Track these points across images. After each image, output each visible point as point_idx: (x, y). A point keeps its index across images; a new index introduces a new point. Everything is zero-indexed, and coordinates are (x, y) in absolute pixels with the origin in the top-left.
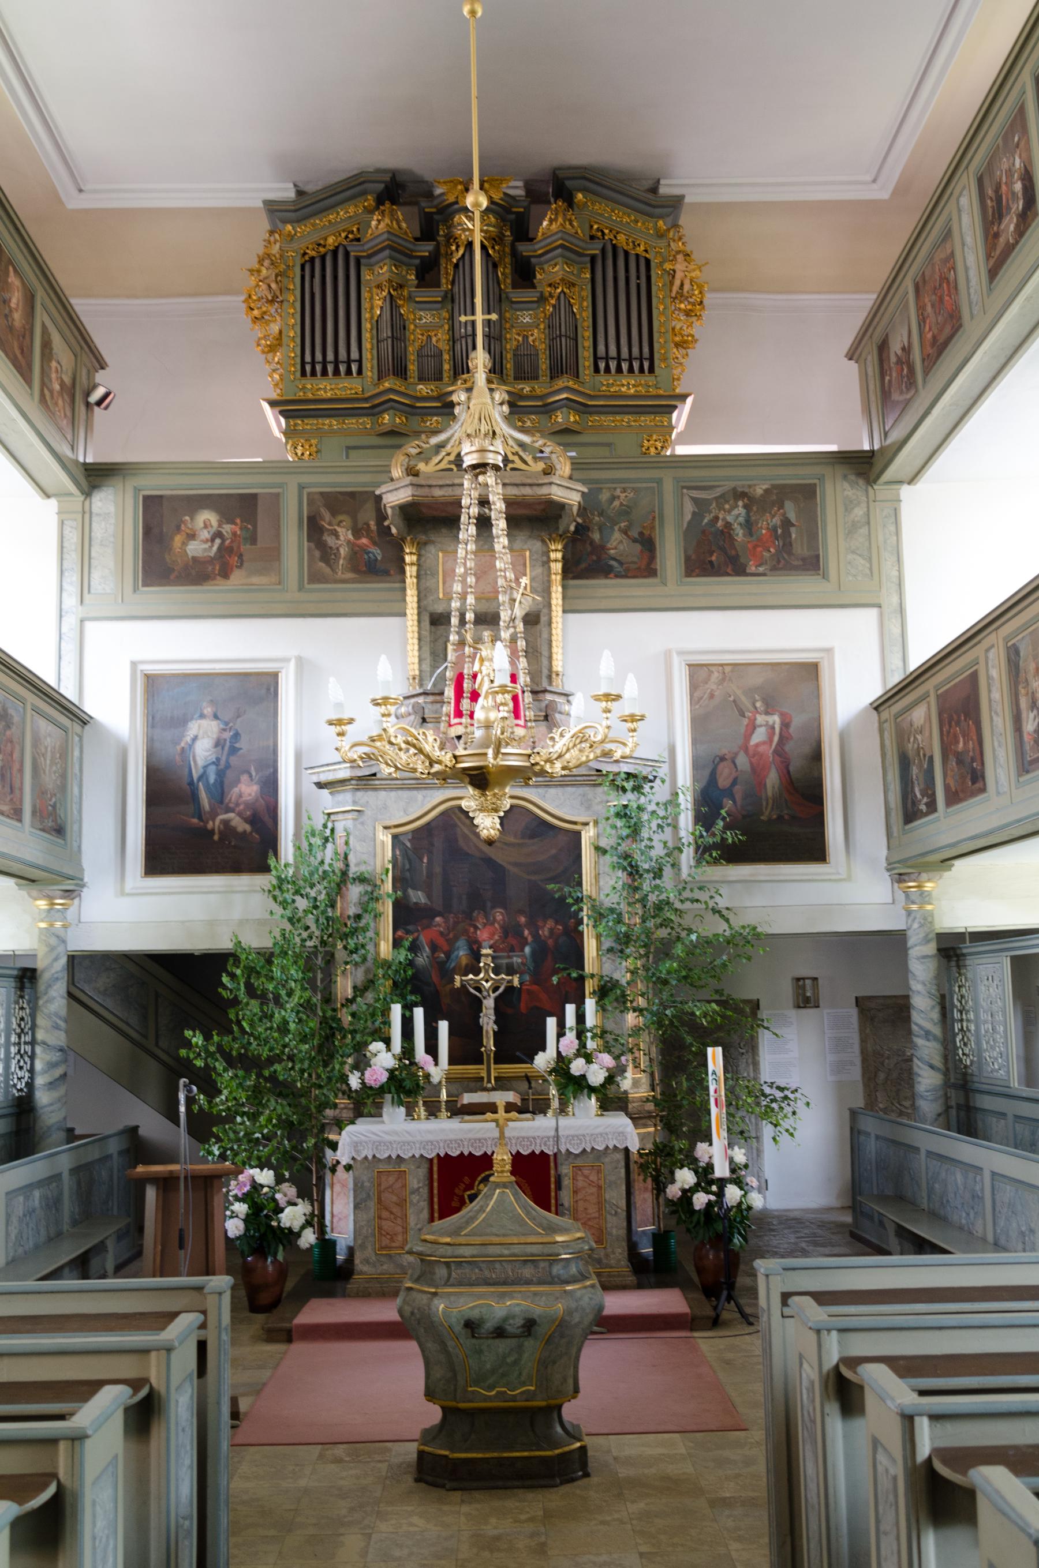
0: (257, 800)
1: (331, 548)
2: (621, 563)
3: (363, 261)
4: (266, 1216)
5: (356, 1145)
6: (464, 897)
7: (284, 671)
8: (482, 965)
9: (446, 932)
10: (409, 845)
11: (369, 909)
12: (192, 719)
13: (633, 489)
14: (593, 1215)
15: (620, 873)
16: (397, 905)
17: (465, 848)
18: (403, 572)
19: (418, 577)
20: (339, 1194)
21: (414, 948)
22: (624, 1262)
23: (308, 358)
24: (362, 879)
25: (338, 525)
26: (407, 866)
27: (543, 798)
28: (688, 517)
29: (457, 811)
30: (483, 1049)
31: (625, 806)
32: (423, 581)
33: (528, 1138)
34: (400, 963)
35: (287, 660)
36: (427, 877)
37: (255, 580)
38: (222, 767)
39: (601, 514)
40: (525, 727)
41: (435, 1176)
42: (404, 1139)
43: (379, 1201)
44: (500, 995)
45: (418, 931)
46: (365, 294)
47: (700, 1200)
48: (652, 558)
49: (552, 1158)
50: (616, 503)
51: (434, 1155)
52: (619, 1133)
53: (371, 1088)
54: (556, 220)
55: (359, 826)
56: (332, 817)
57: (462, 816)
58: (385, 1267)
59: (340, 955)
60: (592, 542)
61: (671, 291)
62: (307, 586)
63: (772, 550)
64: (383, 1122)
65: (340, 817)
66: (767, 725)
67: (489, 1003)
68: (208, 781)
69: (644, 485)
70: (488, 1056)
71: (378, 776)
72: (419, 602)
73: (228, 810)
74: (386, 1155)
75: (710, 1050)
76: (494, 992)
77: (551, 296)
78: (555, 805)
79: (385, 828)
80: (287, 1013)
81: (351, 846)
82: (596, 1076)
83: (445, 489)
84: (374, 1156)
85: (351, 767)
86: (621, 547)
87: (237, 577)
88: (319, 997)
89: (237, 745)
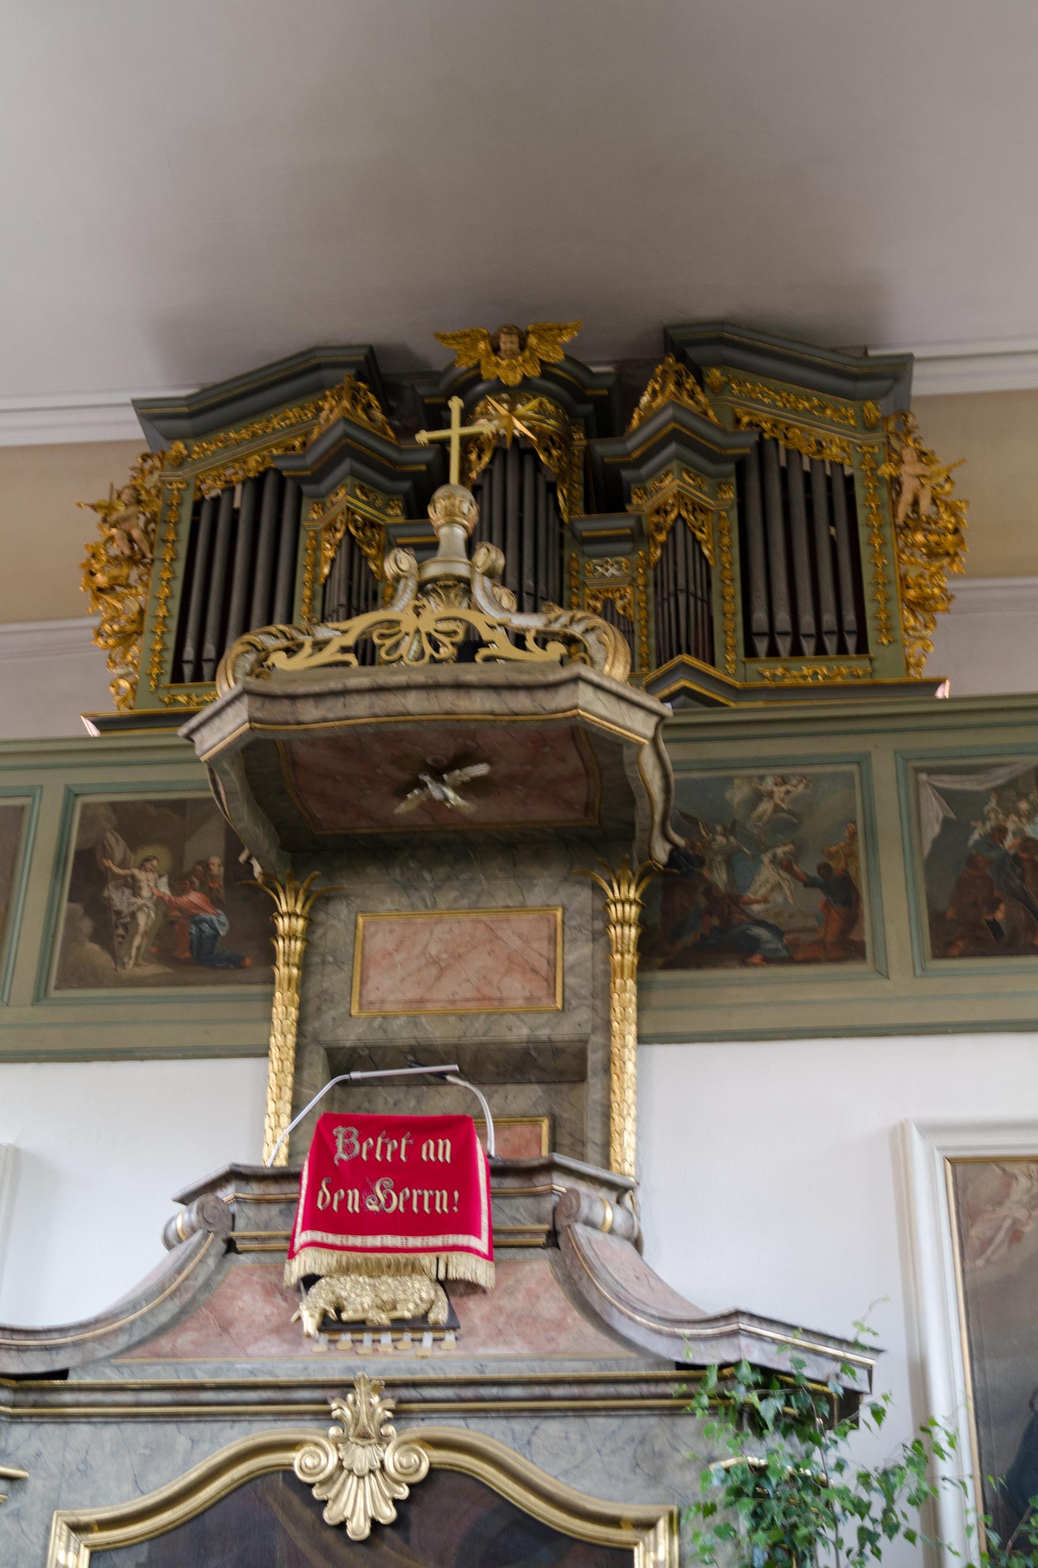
1: (119, 913)
2: (778, 932)
3: (306, 489)
13: (803, 777)
18: (270, 957)
19: (305, 965)
23: (189, 653)
25: (141, 867)
28: (933, 830)
31: (761, 1471)
39: (730, 830)
40: (489, 1257)
46: (304, 542)
50: (765, 807)
54: (663, 388)
57: (296, 1500)
60: (710, 889)
61: (895, 516)
62: (53, 993)
69: (829, 769)
71: (72, 1380)
72: (301, 1022)
77: (659, 528)
78: (563, 1469)
79: (77, 1528)
83: (330, 703)
86: (778, 898)
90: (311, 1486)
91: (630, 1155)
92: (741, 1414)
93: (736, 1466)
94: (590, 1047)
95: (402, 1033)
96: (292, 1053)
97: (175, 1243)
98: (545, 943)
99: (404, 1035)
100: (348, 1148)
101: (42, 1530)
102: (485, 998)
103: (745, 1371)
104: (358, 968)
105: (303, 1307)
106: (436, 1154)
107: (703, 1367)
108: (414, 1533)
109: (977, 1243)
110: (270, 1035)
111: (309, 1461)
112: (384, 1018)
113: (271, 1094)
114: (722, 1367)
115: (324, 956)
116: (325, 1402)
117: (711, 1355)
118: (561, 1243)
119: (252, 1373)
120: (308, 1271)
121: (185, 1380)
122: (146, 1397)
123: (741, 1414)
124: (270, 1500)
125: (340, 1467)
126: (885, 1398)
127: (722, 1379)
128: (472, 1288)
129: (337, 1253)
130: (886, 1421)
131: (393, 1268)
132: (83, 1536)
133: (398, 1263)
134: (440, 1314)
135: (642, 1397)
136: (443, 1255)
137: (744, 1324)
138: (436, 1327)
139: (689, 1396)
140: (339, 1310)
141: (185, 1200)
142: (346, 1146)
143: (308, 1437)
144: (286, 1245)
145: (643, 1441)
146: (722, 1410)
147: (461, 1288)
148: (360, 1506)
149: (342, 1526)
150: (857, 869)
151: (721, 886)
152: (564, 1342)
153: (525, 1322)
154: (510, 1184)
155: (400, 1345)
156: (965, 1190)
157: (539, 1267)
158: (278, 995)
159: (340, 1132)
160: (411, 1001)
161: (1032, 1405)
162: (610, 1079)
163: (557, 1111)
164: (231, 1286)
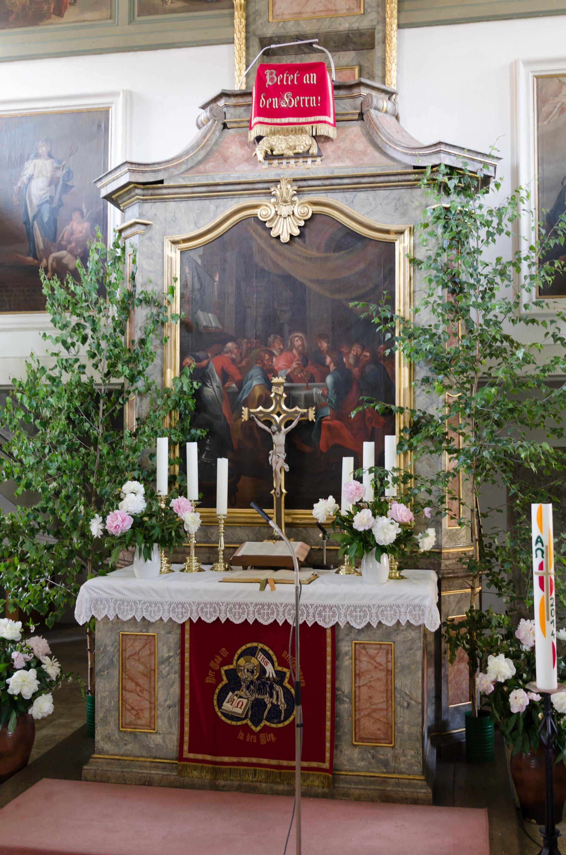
5: (96, 602)
6: (260, 319)
7: (113, 106)
12: (28, 159)
14: (380, 706)
15: (439, 291)
16: (187, 327)
17: (261, 264)
22: (417, 768)
24: (147, 301)
26: (197, 286)
31: (447, 209)
35: (114, 94)
37: (88, 16)
38: (55, 205)
40: (334, 125)
41: (187, 645)
43: (124, 669)
44: (293, 430)
47: (519, 700)
49: (329, 632)
51: (185, 619)
52: (414, 607)
55: (147, 242)
56: (124, 234)
57: (259, 228)
58: (129, 747)
62: (137, 19)
64: (133, 575)
68: (42, 220)
70: (279, 500)
71: (165, 184)
72: (247, 26)
73: (61, 248)
75: (535, 507)
76: (286, 427)
78: (366, 212)
79: (174, 243)
82: (386, 531)
87: (71, 14)
89: (70, 183)
90: (265, 222)
91: (394, 81)
92: (440, 186)
93: (437, 208)
94: (376, 31)
96: (244, 41)
99: (293, 30)
100: (272, 79)
101: (160, 244)
102: (328, 10)
103: (442, 167)
105: (257, 149)
106: (310, 80)
107: (425, 168)
108: (307, 239)
109: (545, 114)
111: (264, 213)
112: (284, 22)
113: (237, 73)
114: (433, 167)
116: (269, 189)
117: (428, 162)
118: (365, 118)
119: (238, 178)
120: (258, 135)
121: (211, 182)
122: (196, 189)
123: (440, 186)
124: (249, 228)
125: (276, 214)
126: (501, 179)
127: (432, 172)
128: (327, 139)
129: (270, 126)
130: (501, 189)
131: (294, 132)
132: (177, 245)
134: (314, 150)
135: (399, 181)
136: (315, 125)
137: (443, 148)
138: (313, 156)
139: (419, 180)
140: (272, 151)
141: (204, 107)
142: (271, 78)
143: (263, 203)
144: (248, 124)
145: (399, 199)
146: (432, 185)
147: (323, 139)
148: (285, 229)
149: (278, 237)
152: (366, 160)
154: (342, 93)
155: (298, 164)
156: (542, 90)
157: (355, 129)
158: (236, 13)
159: (268, 72)
160: (295, 13)
161: (562, 183)
162: (385, 46)
163: (362, 63)
164: (226, 143)
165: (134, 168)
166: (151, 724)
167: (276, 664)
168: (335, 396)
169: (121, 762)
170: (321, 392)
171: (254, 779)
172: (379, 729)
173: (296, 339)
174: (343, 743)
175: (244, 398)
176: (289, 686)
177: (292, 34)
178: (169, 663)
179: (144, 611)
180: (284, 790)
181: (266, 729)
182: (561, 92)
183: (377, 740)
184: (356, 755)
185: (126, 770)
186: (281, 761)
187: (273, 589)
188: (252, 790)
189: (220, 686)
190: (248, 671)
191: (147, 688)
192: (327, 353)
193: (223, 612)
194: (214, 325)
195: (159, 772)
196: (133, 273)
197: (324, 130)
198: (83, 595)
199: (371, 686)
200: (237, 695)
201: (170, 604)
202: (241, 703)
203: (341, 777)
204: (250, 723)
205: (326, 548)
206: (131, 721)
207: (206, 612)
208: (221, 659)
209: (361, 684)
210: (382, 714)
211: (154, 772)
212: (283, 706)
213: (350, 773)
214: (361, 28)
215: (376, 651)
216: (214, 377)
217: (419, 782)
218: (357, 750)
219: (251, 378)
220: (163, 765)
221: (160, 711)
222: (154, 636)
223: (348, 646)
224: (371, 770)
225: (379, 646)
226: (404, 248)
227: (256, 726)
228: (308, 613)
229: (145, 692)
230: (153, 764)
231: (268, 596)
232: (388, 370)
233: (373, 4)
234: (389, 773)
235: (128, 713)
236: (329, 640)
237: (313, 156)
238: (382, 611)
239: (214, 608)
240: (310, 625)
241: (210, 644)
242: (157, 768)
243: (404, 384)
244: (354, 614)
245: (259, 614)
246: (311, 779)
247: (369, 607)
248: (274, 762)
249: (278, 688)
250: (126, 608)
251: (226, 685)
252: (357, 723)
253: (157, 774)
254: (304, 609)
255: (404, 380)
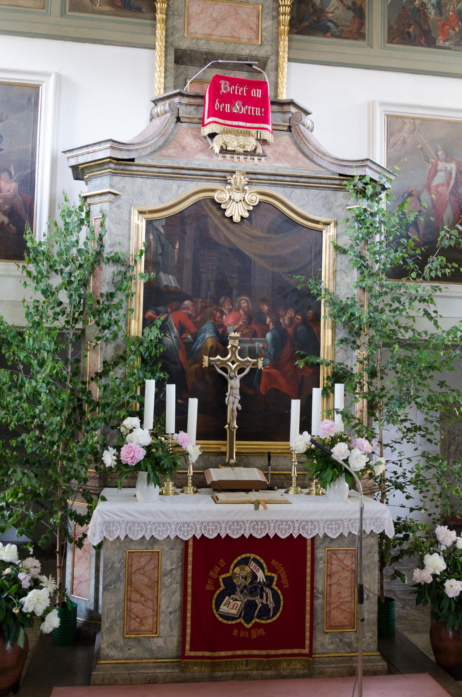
0: (15, 196)
2: (337, 26)
4: (8, 599)
5: (107, 525)
6: (212, 283)
7: (44, 85)
8: (229, 346)
9: (194, 315)
10: (162, 230)
11: (124, 287)
14: (346, 599)
17: (216, 238)
20: (80, 558)
21: (164, 328)
26: (160, 251)
27: (289, 197)
29: (209, 203)
30: (227, 426)
32: (170, 20)
33: (287, 522)
34: (151, 340)
35: (48, 75)
36: (178, 262)
40: (272, 133)
41: (190, 559)
42: (158, 520)
43: (130, 583)
44: (245, 376)
45: (167, 312)
48: (362, 24)
49: (309, 543)
51: (188, 537)
52: (377, 519)
53: (127, 465)
55: (115, 209)
56: (89, 201)
57: (214, 208)
58: (133, 651)
59: (92, 330)
63: (456, 29)
65: (97, 199)
66: (446, 170)
67: (235, 384)
70: (231, 433)
71: (136, 162)
72: (166, 36)
74: (140, 536)
78: (302, 204)
79: (141, 212)
80: (39, 382)
81: (107, 227)
84: (126, 537)
85: (111, 147)
86: (337, 12)
88: (69, 370)
94: (269, 60)
95: (203, 46)
97: (155, 116)
98: (255, 18)
99: (204, 47)
100: (226, 88)
101: (128, 212)
104: (186, 18)
106: (256, 94)
107: (353, 177)
110: (155, 41)
115: (174, 11)
117: (356, 172)
122: (163, 170)
129: (223, 126)
133: (244, 131)
135: (328, 184)
136: (259, 130)
137: (368, 163)
138: (259, 155)
145: (326, 198)
148: (236, 211)
150: (365, 5)
151: (318, 4)
153: (284, 156)
156: (390, 126)
157: (285, 137)
158: (158, 25)
159: (222, 82)
164: (181, 134)
165: (115, 145)
166: (155, 630)
167: (266, 570)
168: (273, 349)
169: (126, 665)
170: (262, 345)
171: (247, 668)
172: (345, 618)
173: (243, 301)
174: (317, 632)
175: (198, 348)
176: (276, 588)
177: (202, 50)
178: (172, 575)
179: (153, 531)
180: (271, 675)
181: (257, 625)
182: (403, 129)
183: (343, 627)
184: (327, 640)
185: (132, 672)
186: (269, 651)
187: (265, 508)
188: (245, 678)
189: (218, 592)
190: (242, 577)
191: (151, 598)
192: (267, 314)
193: (223, 528)
194: (174, 285)
195: (163, 671)
196: (100, 235)
197: (267, 135)
198: (96, 519)
199: (340, 584)
200: (232, 599)
201: (177, 524)
202: (236, 605)
203: (317, 659)
204: (243, 622)
205: (270, 472)
206: (135, 629)
207: (209, 530)
208: (219, 569)
209: (332, 583)
210: (347, 606)
211: (158, 671)
212: (271, 605)
213: (323, 656)
214: (258, 55)
215: (344, 556)
216: (172, 329)
217: (376, 657)
218: (328, 636)
219: (204, 332)
220: (165, 664)
221: (162, 617)
222: (159, 552)
223: (323, 553)
224: (338, 651)
225: (345, 552)
226: (330, 236)
227: (248, 624)
228: (294, 527)
229: (149, 601)
230: (156, 664)
231: (262, 514)
232: (315, 331)
233: (269, 39)
234: (352, 652)
235: (133, 621)
236: (309, 549)
237: (259, 155)
238: (352, 523)
239: (216, 526)
240: (295, 537)
241: (209, 556)
242: (160, 667)
243: (328, 342)
244: (331, 526)
245: (254, 529)
246: (294, 663)
247: (342, 520)
248: (264, 652)
249: (268, 590)
250: (136, 528)
251: (223, 590)
252: (328, 615)
253: (161, 673)
254: (291, 524)
255: (328, 339)
